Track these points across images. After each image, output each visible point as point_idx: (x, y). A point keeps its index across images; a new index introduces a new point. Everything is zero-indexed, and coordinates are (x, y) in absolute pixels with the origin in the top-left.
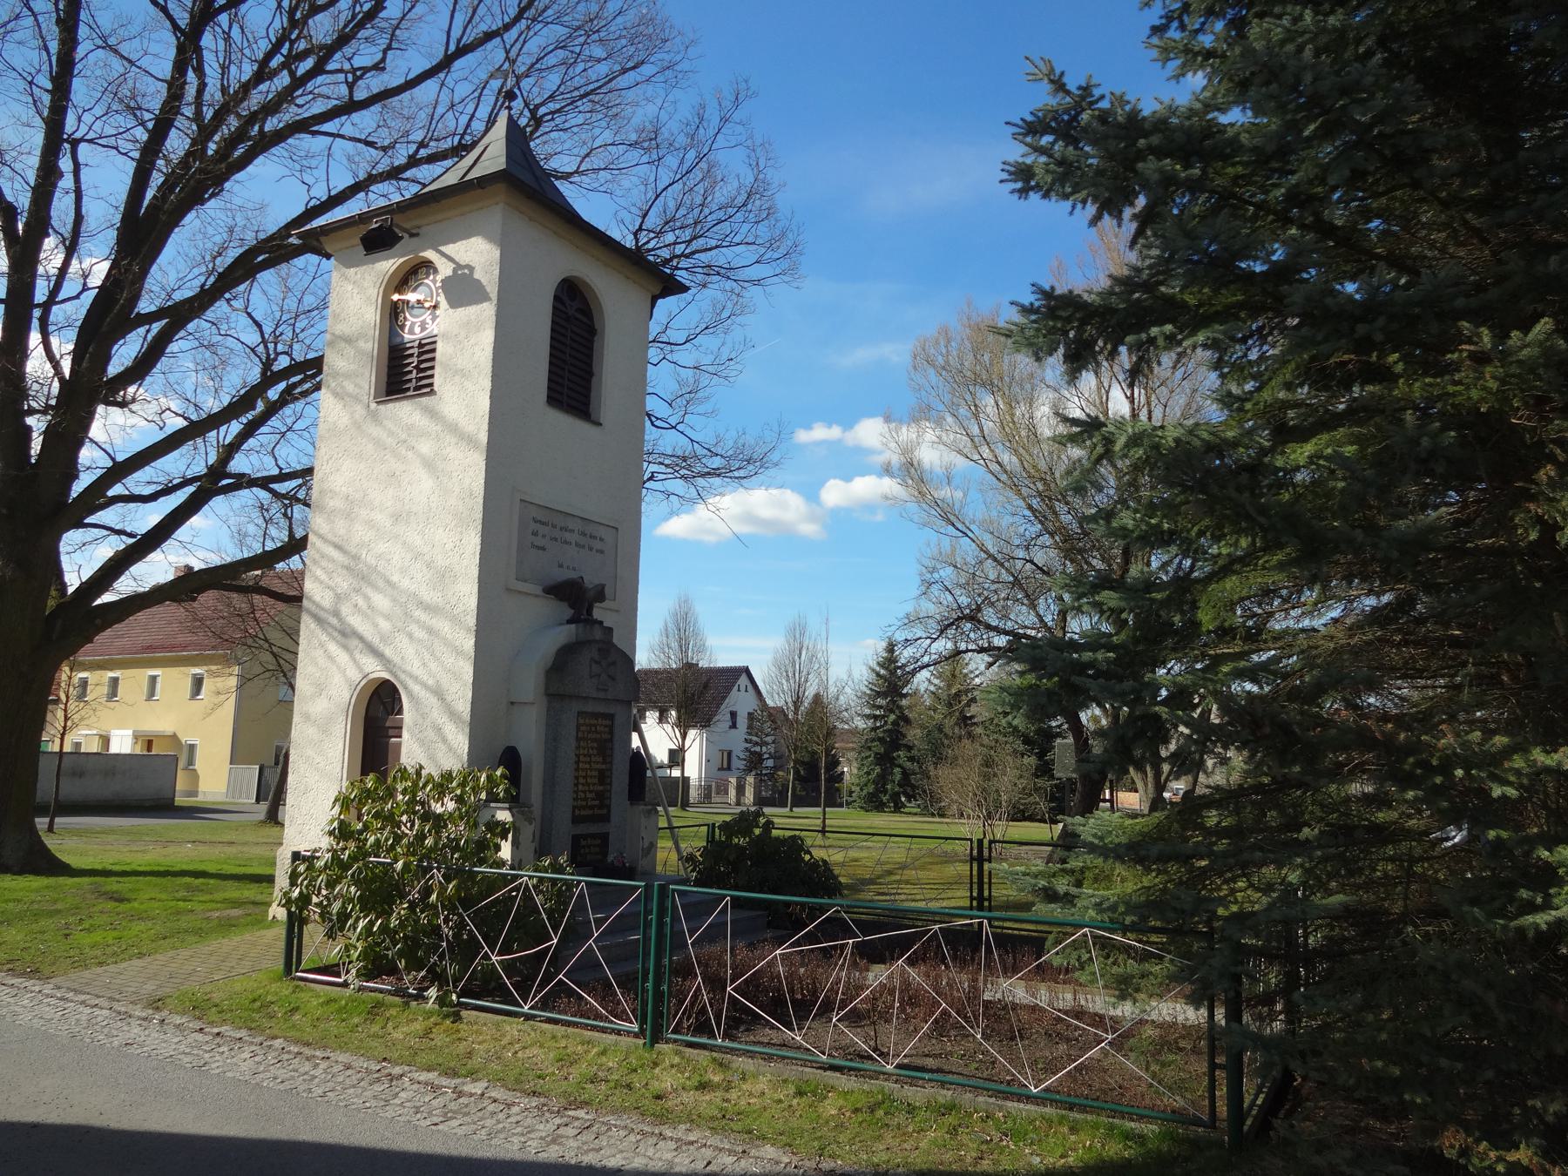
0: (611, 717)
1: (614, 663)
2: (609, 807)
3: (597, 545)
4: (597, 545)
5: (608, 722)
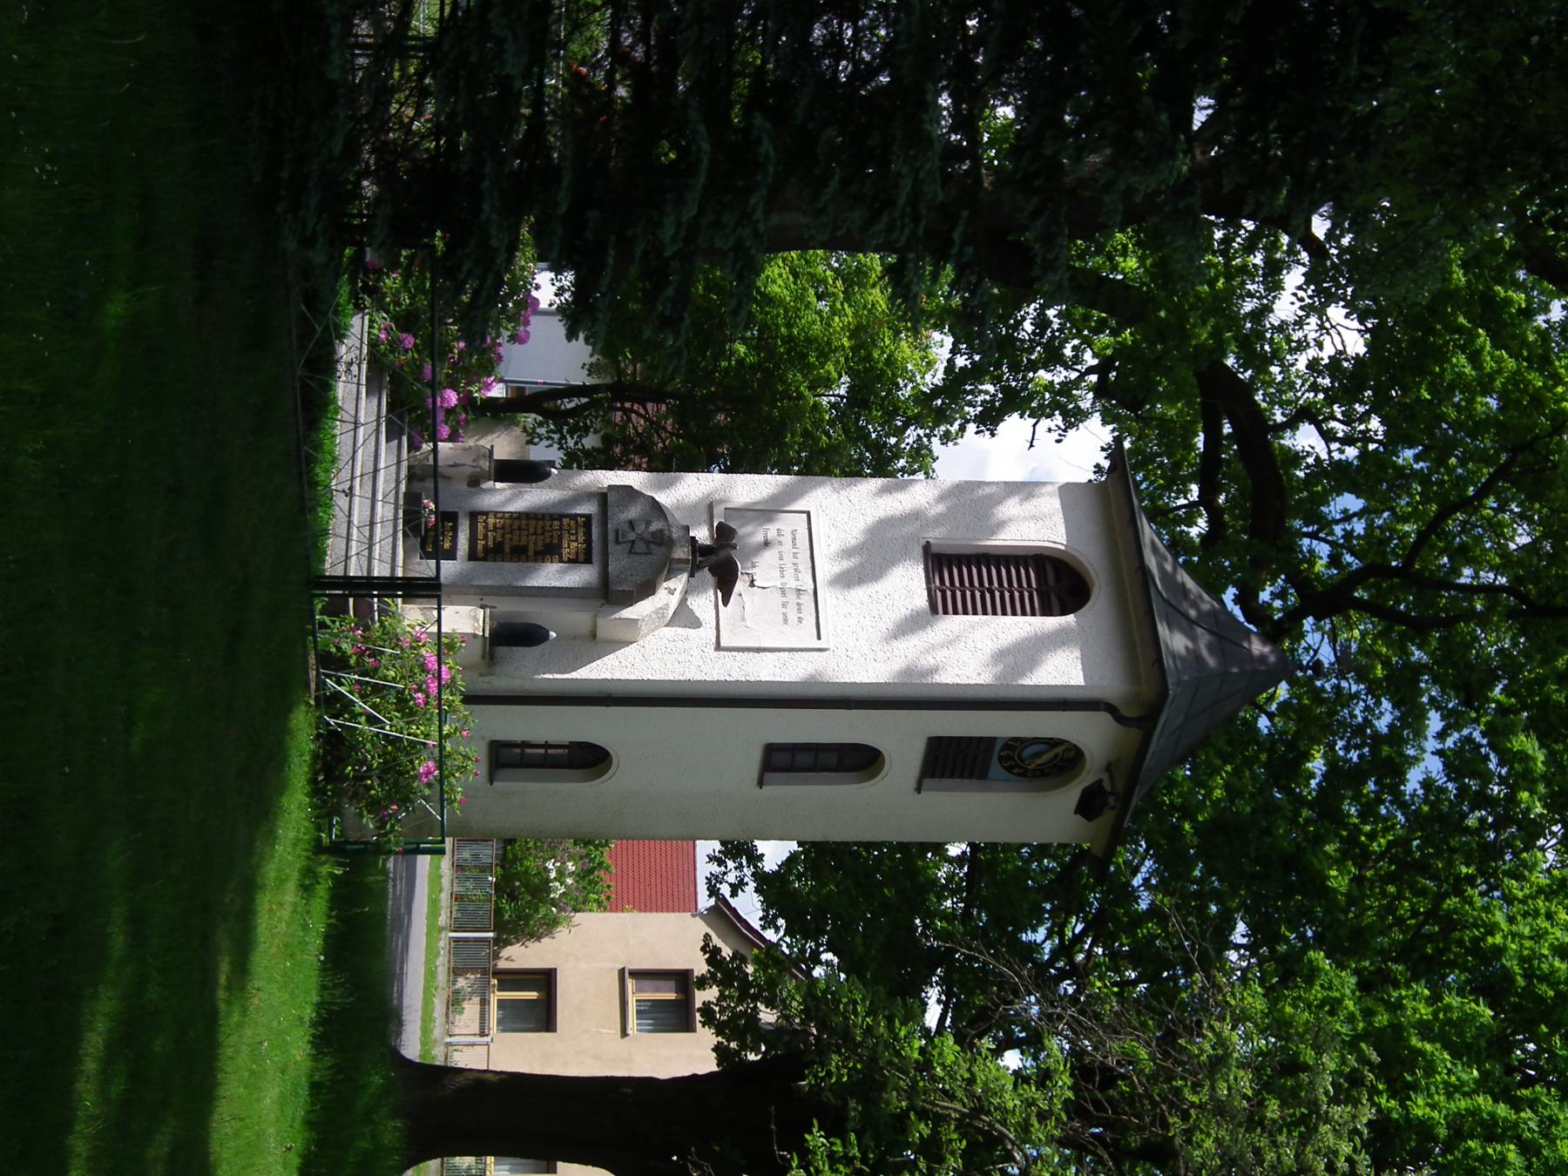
2: (485, 559)
3: (793, 615)
4: (793, 615)
5: (581, 558)
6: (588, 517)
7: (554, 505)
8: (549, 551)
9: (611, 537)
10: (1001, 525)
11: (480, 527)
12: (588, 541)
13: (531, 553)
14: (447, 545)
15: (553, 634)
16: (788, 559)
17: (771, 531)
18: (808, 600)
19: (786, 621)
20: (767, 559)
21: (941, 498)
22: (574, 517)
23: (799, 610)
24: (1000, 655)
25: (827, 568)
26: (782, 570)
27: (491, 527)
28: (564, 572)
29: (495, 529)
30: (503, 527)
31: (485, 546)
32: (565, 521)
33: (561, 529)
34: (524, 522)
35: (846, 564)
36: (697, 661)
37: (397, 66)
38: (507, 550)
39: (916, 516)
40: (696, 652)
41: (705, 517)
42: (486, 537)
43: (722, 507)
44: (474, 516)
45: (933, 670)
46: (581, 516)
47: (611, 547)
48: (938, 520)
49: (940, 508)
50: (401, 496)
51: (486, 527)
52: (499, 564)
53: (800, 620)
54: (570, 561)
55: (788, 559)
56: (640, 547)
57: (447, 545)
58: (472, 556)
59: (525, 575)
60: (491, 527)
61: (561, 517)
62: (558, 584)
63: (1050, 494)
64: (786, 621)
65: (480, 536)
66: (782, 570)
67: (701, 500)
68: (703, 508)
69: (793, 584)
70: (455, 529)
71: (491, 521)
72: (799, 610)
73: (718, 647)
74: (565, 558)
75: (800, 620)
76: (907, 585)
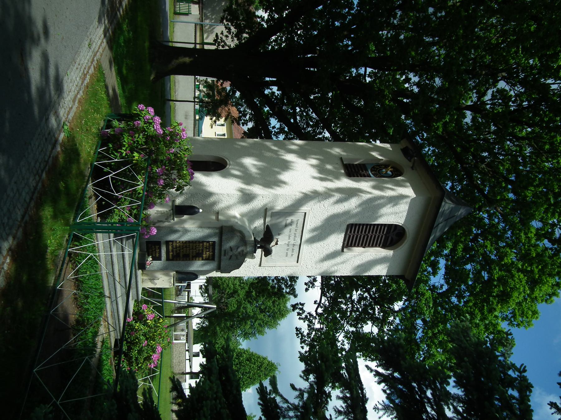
1: (237, 258)
2: (172, 260)
3: (290, 253)
4: (290, 253)
5: (211, 258)
6: (214, 242)
7: (200, 238)
8: (198, 256)
9: (223, 253)
10: (380, 216)
11: (170, 247)
12: (214, 251)
13: (191, 256)
14: (157, 255)
15: (201, 210)
17: (289, 220)
19: (287, 256)
20: (286, 231)
21: (360, 205)
22: (209, 242)
23: (293, 251)
24: (359, 266)
25: (306, 236)
26: (289, 237)
27: (174, 247)
28: (203, 265)
30: (179, 247)
32: (205, 244)
33: (203, 247)
34: (188, 244)
35: (315, 233)
36: (252, 270)
37: (118, 390)
38: (181, 255)
39: (346, 213)
40: (252, 267)
41: (263, 214)
42: (173, 251)
43: (270, 212)
44: (167, 243)
45: (334, 272)
47: (222, 257)
48: (356, 215)
49: (358, 210)
52: (178, 262)
53: (292, 255)
54: (206, 259)
55: (293, 232)
57: (157, 255)
58: (168, 259)
59: (189, 266)
61: (203, 242)
62: (201, 269)
63: (406, 203)
64: (287, 256)
65: (170, 250)
66: (289, 237)
68: (263, 211)
69: (292, 242)
70: (160, 249)
71: (174, 244)
72: (293, 251)
73: (260, 265)
75: (292, 255)
76: (336, 240)
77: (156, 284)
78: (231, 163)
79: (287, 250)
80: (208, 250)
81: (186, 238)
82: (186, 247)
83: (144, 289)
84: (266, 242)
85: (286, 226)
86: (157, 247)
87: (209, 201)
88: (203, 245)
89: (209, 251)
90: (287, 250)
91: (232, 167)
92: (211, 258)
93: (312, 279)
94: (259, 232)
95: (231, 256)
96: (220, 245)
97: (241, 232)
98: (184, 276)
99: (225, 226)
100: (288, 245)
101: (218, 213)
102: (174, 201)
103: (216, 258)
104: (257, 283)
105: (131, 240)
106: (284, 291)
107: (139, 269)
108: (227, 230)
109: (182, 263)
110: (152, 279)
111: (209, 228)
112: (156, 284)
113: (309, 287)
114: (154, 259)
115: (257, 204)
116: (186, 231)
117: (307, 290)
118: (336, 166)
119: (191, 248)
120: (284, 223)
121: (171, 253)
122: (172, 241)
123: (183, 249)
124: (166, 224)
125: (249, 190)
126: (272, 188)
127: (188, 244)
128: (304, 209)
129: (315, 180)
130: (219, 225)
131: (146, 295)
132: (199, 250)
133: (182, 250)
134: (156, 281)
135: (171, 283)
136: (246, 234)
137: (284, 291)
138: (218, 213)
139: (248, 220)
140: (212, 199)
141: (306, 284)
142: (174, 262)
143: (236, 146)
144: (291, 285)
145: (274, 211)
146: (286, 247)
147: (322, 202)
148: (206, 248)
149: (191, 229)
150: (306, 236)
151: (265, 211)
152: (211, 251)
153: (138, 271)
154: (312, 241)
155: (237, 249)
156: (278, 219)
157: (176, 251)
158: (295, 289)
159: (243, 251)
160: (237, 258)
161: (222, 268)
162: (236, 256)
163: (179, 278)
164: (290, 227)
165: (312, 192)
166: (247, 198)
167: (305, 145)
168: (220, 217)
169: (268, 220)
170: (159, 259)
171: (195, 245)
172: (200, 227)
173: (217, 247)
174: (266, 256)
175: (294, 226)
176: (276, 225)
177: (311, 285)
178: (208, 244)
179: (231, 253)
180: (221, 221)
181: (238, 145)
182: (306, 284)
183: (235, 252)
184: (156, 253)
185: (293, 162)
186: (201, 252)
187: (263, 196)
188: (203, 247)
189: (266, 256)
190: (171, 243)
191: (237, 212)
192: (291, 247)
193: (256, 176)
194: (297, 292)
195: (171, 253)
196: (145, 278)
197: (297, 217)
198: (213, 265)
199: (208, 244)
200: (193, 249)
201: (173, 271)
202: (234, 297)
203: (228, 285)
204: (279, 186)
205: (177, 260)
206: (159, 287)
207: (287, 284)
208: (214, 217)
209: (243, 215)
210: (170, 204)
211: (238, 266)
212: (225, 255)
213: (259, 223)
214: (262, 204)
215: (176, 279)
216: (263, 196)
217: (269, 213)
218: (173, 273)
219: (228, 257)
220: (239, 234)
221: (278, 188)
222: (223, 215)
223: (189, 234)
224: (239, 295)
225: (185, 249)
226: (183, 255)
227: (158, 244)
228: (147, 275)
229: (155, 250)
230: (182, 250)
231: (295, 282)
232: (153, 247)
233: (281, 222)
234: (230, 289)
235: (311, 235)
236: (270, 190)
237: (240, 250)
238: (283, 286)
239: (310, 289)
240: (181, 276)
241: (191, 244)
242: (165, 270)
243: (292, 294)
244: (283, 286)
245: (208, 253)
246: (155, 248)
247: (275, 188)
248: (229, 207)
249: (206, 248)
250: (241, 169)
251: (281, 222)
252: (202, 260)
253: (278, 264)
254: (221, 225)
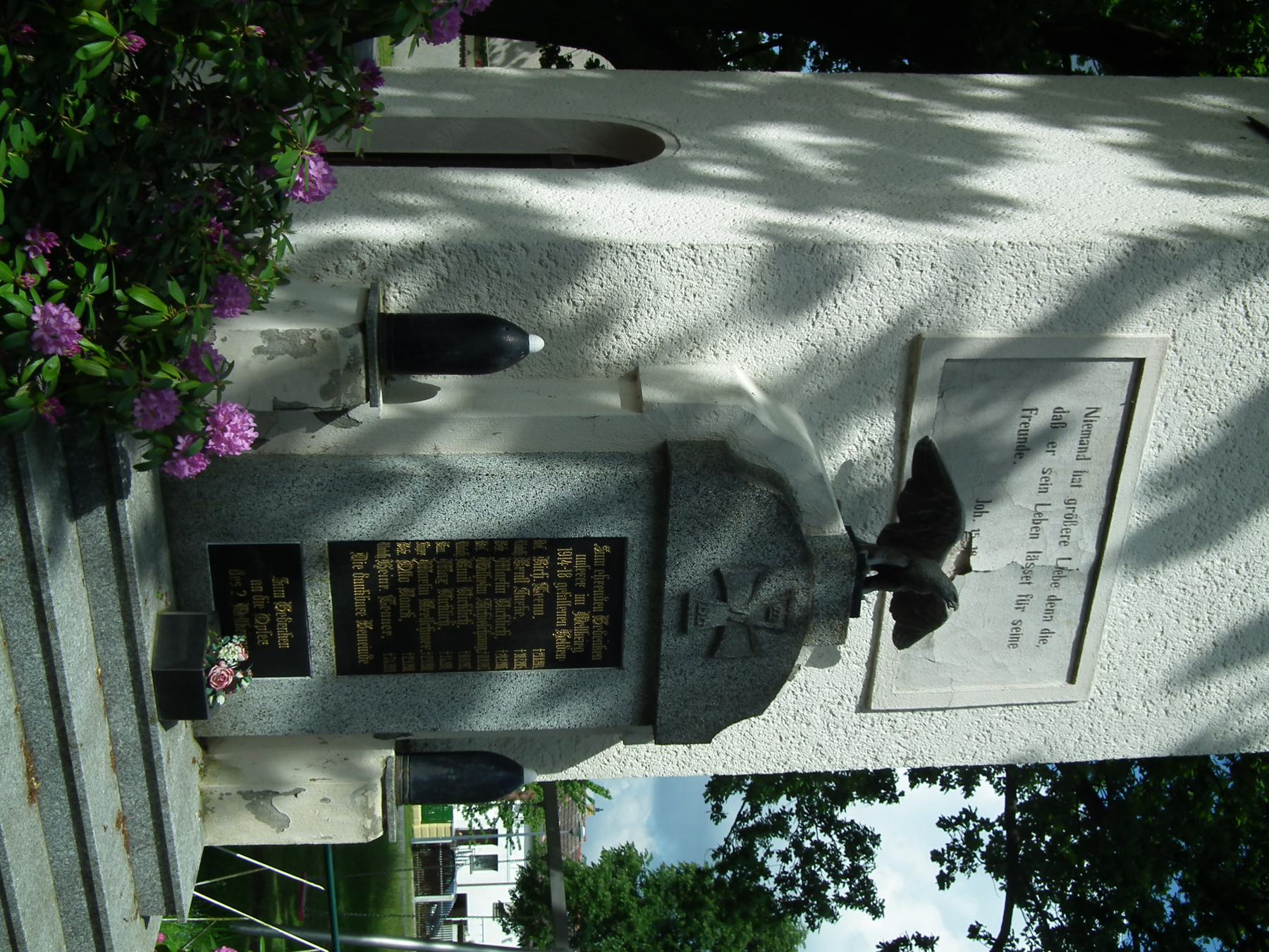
0: (613, 658)
1: (753, 645)
2: (375, 668)
3: (1032, 623)
4: (1032, 623)
5: (598, 650)
6: (619, 545)
8: (522, 638)
9: (669, 615)
12: (615, 609)
13: (482, 644)
14: (284, 638)
15: (536, 343)
16: (1060, 487)
17: (1044, 406)
18: (1072, 593)
19: (1014, 640)
20: (1025, 480)
22: (584, 545)
23: (1049, 613)
25: (1130, 516)
26: (1038, 520)
27: (383, 582)
28: (550, 698)
29: (395, 585)
30: (413, 582)
31: (373, 635)
34: (463, 563)
36: (817, 733)
40: (817, 717)
41: (894, 380)
42: (373, 610)
46: (602, 541)
47: (670, 642)
50: (149, 684)
51: (371, 583)
53: (1045, 635)
54: (575, 660)
55: (1060, 487)
56: (735, 642)
57: (284, 638)
58: (347, 664)
59: (467, 704)
60: (383, 582)
61: (553, 545)
64: (1014, 640)
65: (360, 607)
66: (1038, 520)
67: (883, 340)
68: (895, 352)
69: (1051, 554)
70: (297, 596)
71: (382, 565)
72: (1049, 613)
73: (864, 705)
74: (561, 654)
75: (1045, 635)
77: (283, 823)
78: (684, 140)
79: (1021, 603)
80: (580, 599)
81: (444, 522)
82: (453, 583)
83: (215, 860)
84: (909, 556)
85: (1023, 450)
86: (280, 584)
87: (579, 296)
88: (553, 568)
89: (587, 607)
90: (1021, 603)
91: (692, 152)
92: (597, 655)
93: (959, 834)
94: (867, 498)
95: (720, 631)
96: (657, 565)
97: (775, 480)
98: (442, 771)
99: (681, 444)
100: (1027, 574)
101: (632, 377)
102: (370, 294)
103: (631, 654)
104: (721, 868)
105: (103, 511)
106: (830, 894)
107: (169, 717)
108: (688, 465)
109: (430, 683)
110: (260, 798)
111: (586, 457)
112: (283, 823)
113: (951, 869)
114: (263, 661)
115: (857, 315)
116: (445, 478)
117: (944, 881)
118: (1242, 145)
119: (482, 587)
120: (1010, 435)
121: (364, 626)
122: (369, 547)
123: (433, 595)
124: (329, 437)
125: (811, 230)
126: (946, 222)
127: (463, 563)
128: (1137, 333)
129: (1163, 192)
130: (643, 442)
131: (297, 923)
132: (530, 600)
133: (427, 604)
134: (284, 806)
135: (369, 813)
136: (805, 500)
137: (830, 894)
138: (632, 377)
139: (808, 421)
140: (592, 289)
141: (936, 856)
142: (387, 683)
143: (698, 93)
144: (855, 871)
145: (961, 352)
146: (1015, 588)
147: (1242, 292)
148: (571, 584)
149: (471, 470)
150: (1130, 516)
151: (908, 360)
152: (599, 605)
153: (160, 735)
154: (1160, 545)
155: (757, 583)
156: (979, 406)
157: (395, 610)
158: (870, 883)
159: (788, 597)
160: (753, 645)
161: (663, 715)
162: (748, 627)
163: (416, 784)
164: (1043, 460)
165: (1179, 233)
166: (796, 277)
167: (1042, 87)
168: (650, 394)
169: (921, 413)
170: (292, 660)
171: (504, 563)
172: (524, 455)
173: (634, 582)
174: (904, 638)
175: (1067, 449)
176: (970, 444)
177: (959, 862)
178: (581, 559)
179: (717, 616)
180: (654, 408)
181: (704, 89)
182: (936, 856)
183: (746, 606)
184: (272, 626)
185: (1012, 136)
186: (539, 611)
187: (894, 266)
188: (552, 579)
189: (904, 638)
190: (359, 560)
191: (745, 364)
192: (1041, 587)
193: (834, 180)
194: (879, 896)
195: (364, 626)
196: (218, 786)
197: (1093, 393)
198: (617, 690)
199: (581, 559)
200: (491, 594)
201: (382, 737)
202: (614, 934)
203: (594, 895)
204: (980, 214)
205: (399, 671)
206: (299, 839)
207: (840, 866)
208: (614, 400)
209: (777, 392)
210: (351, 305)
211: (754, 699)
212: (682, 628)
213: (863, 445)
214: (892, 310)
215: (401, 789)
216: (894, 266)
217: (930, 369)
218: (378, 759)
219: (699, 637)
220: (763, 489)
221: (977, 221)
222: (662, 381)
223: (467, 492)
224: (631, 928)
225: (446, 593)
226: (430, 617)
227: (286, 564)
228: (231, 770)
229: (269, 609)
230: (427, 604)
231: (869, 854)
232: (257, 585)
233: (997, 426)
234: (600, 905)
235: (1158, 509)
236: (932, 228)
237: (768, 591)
238: (824, 875)
239: (957, 875)
240: (424, 772)
241: (483, 564)
242: (326, 732)
243: (860, 905)
244: (824, 875)
245: (580, 618)
246: (268, 590)
247: (968, 220)
248: (691, 340)
249: (571, 584)
250: (745, 159)
251: (997, 426)
252: (551, 663)
253: (967, 692)
254: (657, 440)
